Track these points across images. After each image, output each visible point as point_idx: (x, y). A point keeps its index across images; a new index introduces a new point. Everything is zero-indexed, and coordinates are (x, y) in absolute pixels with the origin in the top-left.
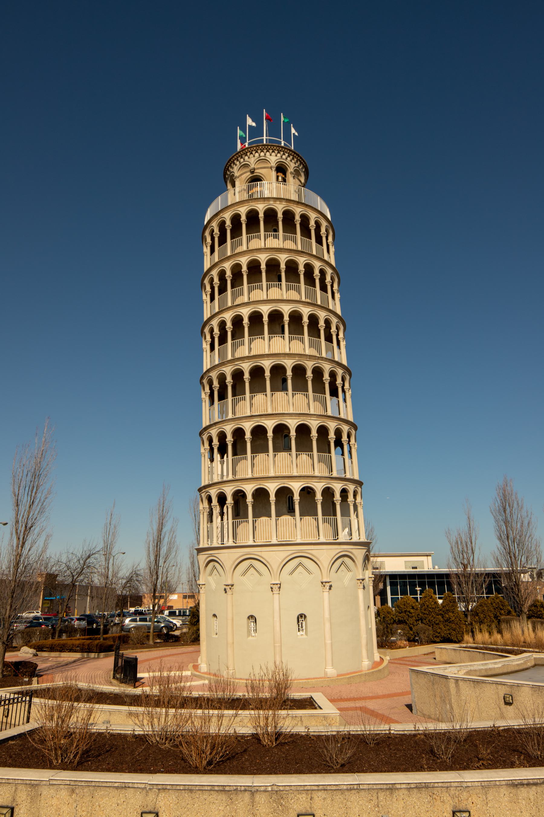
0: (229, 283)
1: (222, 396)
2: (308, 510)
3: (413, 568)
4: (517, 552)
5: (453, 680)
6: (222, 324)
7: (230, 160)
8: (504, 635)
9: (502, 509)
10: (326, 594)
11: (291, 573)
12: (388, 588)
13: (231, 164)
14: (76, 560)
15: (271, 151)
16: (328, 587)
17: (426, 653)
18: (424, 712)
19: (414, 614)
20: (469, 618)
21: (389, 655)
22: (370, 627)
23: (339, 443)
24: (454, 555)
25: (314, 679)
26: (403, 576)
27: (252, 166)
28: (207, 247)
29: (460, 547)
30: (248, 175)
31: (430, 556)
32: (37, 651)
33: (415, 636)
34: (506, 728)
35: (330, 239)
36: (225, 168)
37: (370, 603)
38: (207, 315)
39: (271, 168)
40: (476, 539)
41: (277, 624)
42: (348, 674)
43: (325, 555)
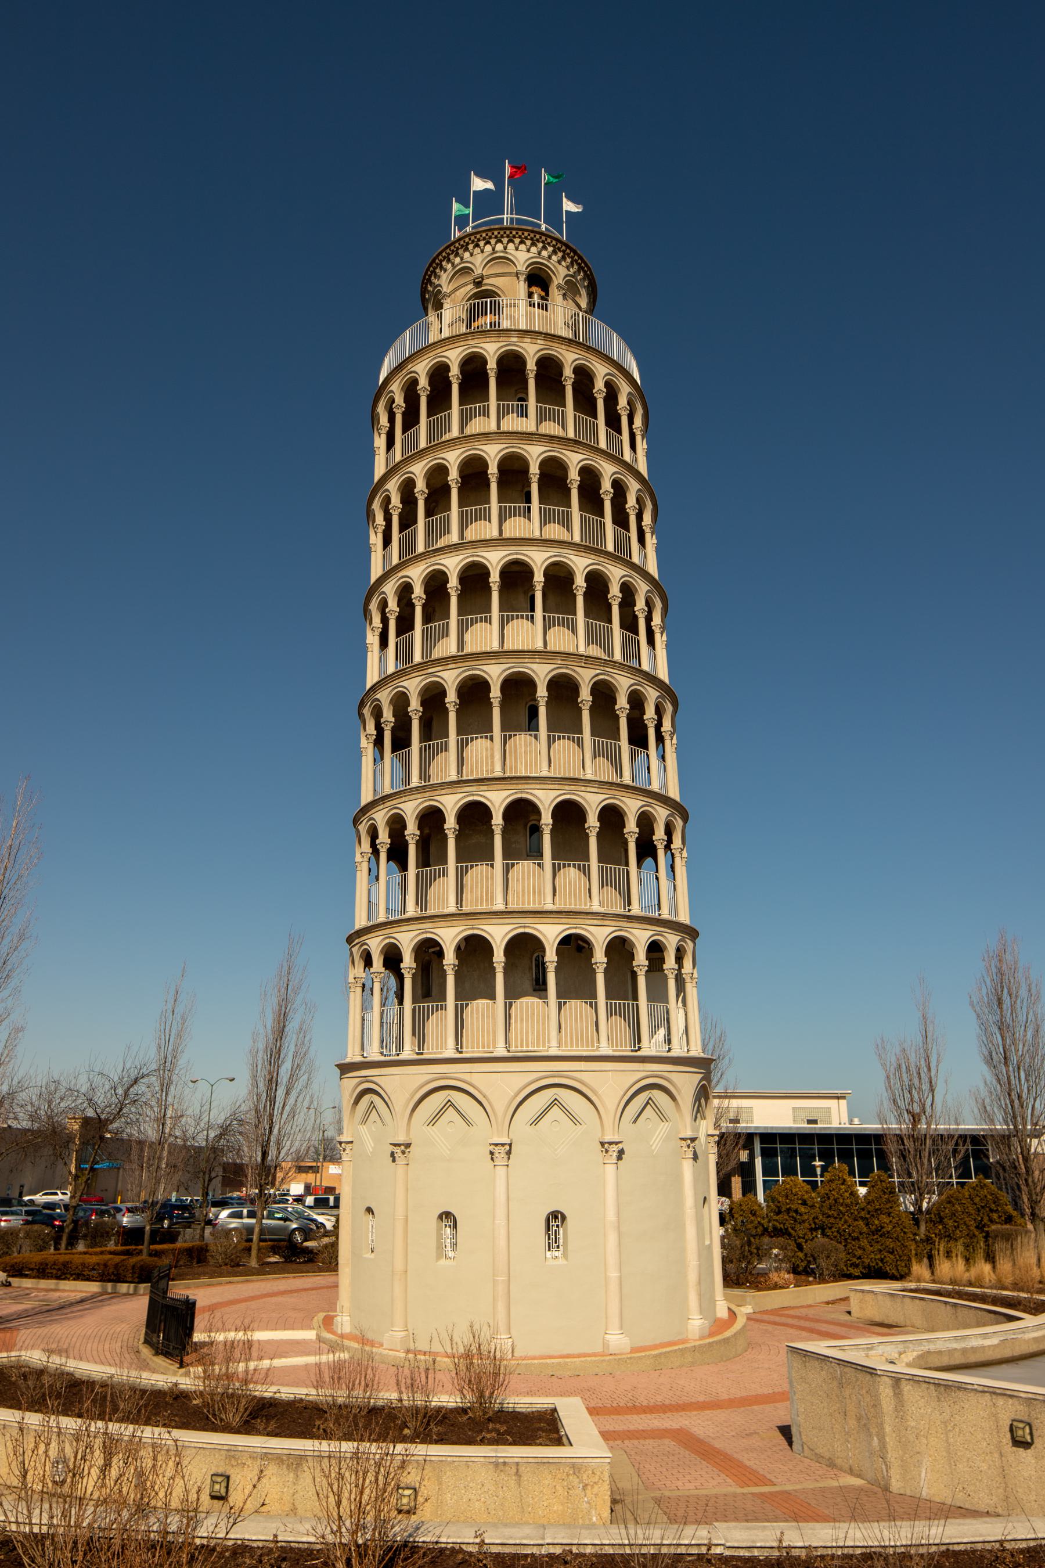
0: (421, 504)
1: (401, 742)
2: (576, 983)
3: (810, 1122)
4: (1026, 1090)
5: (887, 1379)
6: (406, 589)
7: (434, 261)
8: (998, 1266)
10: (610, 1169)
12: (758, 1162)
13: (435, 268)
14: (107, 1087)
16: (615, 1154)
18: (819, 1451)
19: (806, 1217)
20: (923, 1228)
21: (750, 1303)
22: (707, 1242)
23: (646, 850)
24: (893, 1094)
25: (579, 1356)
26: (787, 1137)
27: (478, 271)
28: (380, 434)
30: (470, 289)
31: (844, 1098)
32: (9, 1276)
33: (809, 1262)
34: (1032, 1544)
35: (647, 519)
36: (424, 278)
37: (709, 1192)
38: (372, 677)
39: (517, 275)
40: (938, 1061)
41: (502, 1233)
42: (655, 1347)
43: (612, 1083)
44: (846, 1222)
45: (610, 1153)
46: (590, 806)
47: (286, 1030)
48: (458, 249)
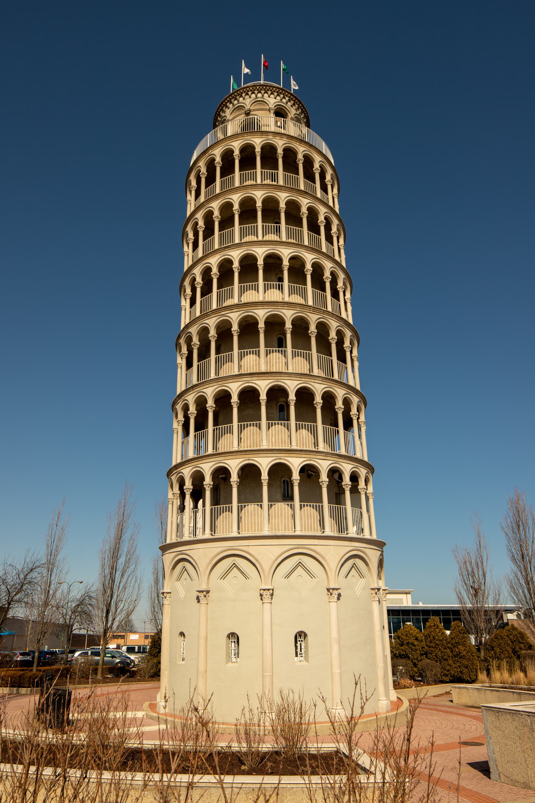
2: (311, 495)
6: (207, 272)
7: (222, 103)
8: (528, 673)
9: (514, 525)
10: (333, 605)
11: (288, 576)
14: (14, 574)
15: (269, 92)
16: (336, 596)
17: (435, 694)
20: (482, 654)
27: (248, 107)
28: (186, 299)
29: (469, 567)
30: (242, 117)
31: (409, 593)
36: (216, 113)
38: (181, 387)
39: (269, 110)
44: (440, 650)
45: (333, 595)
46: (311, 319)
47: (123, 538)
48: (236, 96)
